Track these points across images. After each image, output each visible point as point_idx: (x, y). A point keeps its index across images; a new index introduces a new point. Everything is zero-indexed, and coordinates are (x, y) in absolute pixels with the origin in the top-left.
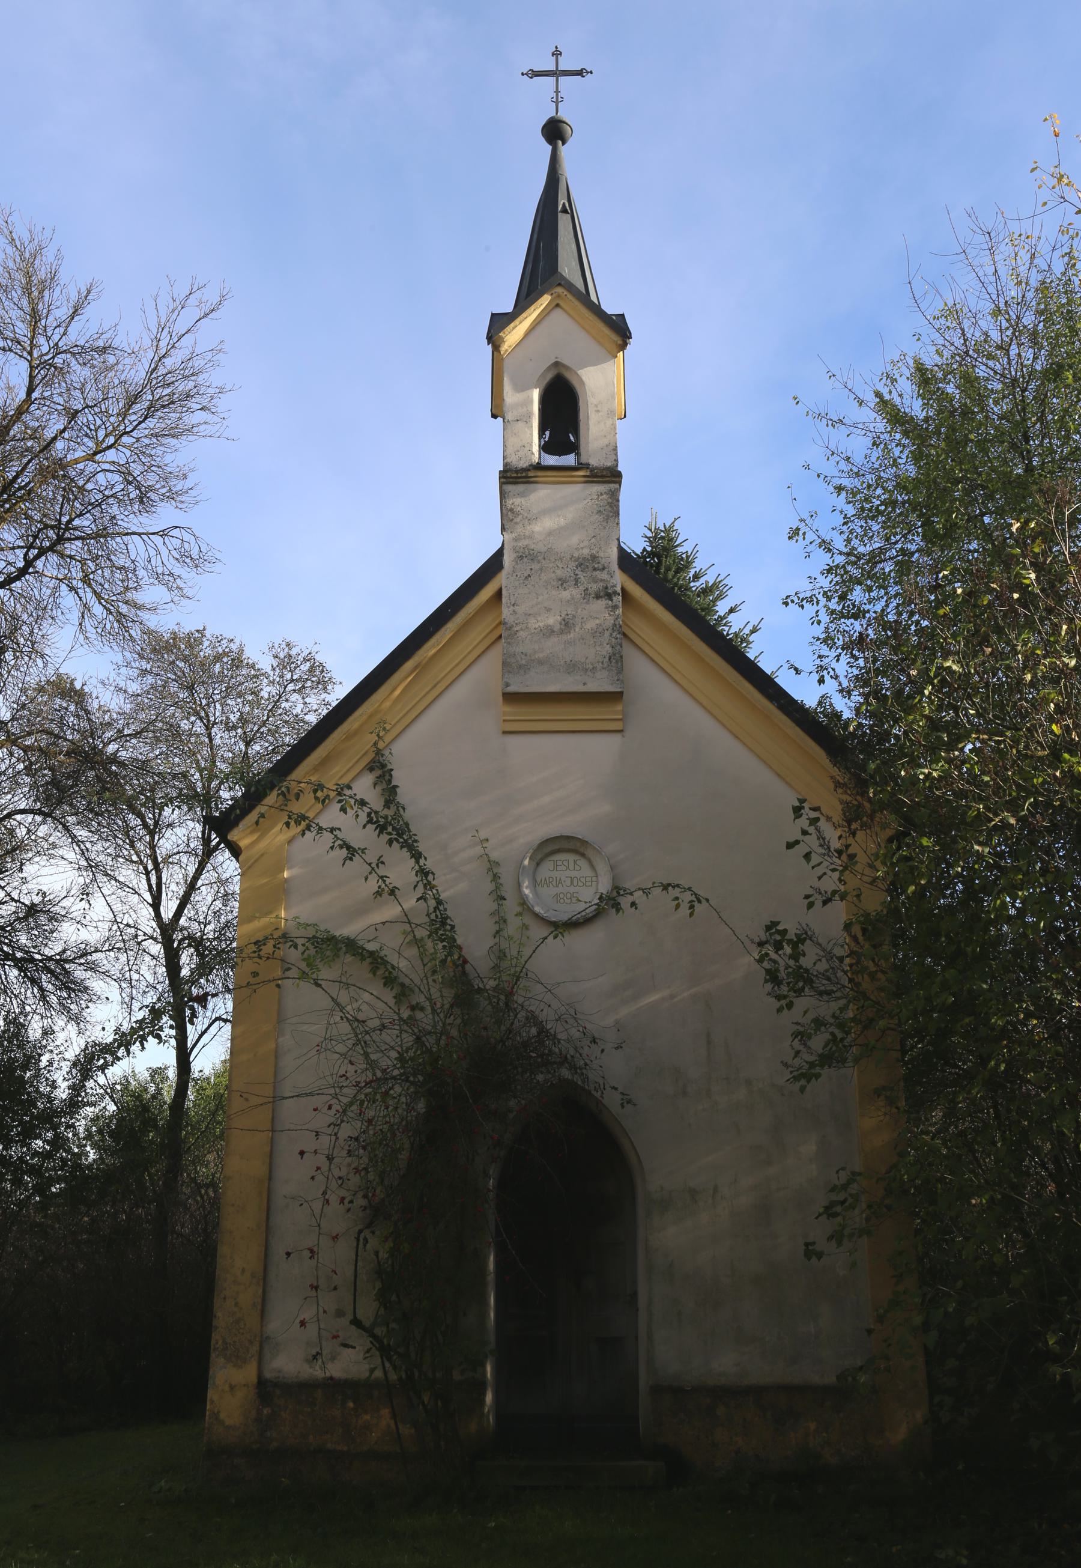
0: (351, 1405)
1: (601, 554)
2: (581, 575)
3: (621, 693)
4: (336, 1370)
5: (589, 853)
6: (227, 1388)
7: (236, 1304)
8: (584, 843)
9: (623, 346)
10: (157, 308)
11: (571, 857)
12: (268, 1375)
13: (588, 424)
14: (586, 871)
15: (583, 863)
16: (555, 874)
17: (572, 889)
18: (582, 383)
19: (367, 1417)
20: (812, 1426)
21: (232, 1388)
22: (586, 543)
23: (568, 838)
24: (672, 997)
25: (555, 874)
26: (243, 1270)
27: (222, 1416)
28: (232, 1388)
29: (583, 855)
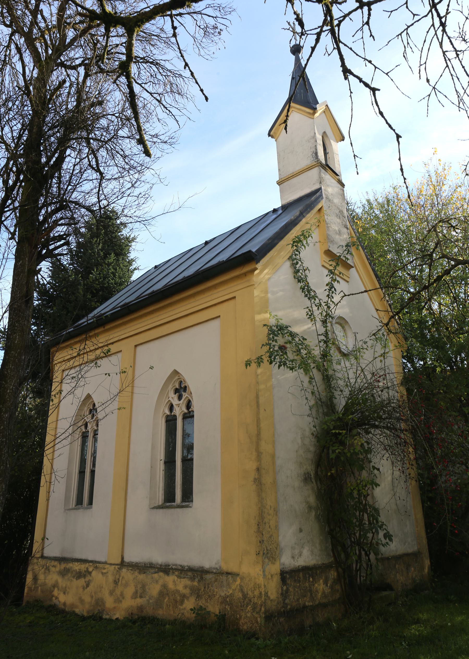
6: (270, 577)
21: (272, 576)
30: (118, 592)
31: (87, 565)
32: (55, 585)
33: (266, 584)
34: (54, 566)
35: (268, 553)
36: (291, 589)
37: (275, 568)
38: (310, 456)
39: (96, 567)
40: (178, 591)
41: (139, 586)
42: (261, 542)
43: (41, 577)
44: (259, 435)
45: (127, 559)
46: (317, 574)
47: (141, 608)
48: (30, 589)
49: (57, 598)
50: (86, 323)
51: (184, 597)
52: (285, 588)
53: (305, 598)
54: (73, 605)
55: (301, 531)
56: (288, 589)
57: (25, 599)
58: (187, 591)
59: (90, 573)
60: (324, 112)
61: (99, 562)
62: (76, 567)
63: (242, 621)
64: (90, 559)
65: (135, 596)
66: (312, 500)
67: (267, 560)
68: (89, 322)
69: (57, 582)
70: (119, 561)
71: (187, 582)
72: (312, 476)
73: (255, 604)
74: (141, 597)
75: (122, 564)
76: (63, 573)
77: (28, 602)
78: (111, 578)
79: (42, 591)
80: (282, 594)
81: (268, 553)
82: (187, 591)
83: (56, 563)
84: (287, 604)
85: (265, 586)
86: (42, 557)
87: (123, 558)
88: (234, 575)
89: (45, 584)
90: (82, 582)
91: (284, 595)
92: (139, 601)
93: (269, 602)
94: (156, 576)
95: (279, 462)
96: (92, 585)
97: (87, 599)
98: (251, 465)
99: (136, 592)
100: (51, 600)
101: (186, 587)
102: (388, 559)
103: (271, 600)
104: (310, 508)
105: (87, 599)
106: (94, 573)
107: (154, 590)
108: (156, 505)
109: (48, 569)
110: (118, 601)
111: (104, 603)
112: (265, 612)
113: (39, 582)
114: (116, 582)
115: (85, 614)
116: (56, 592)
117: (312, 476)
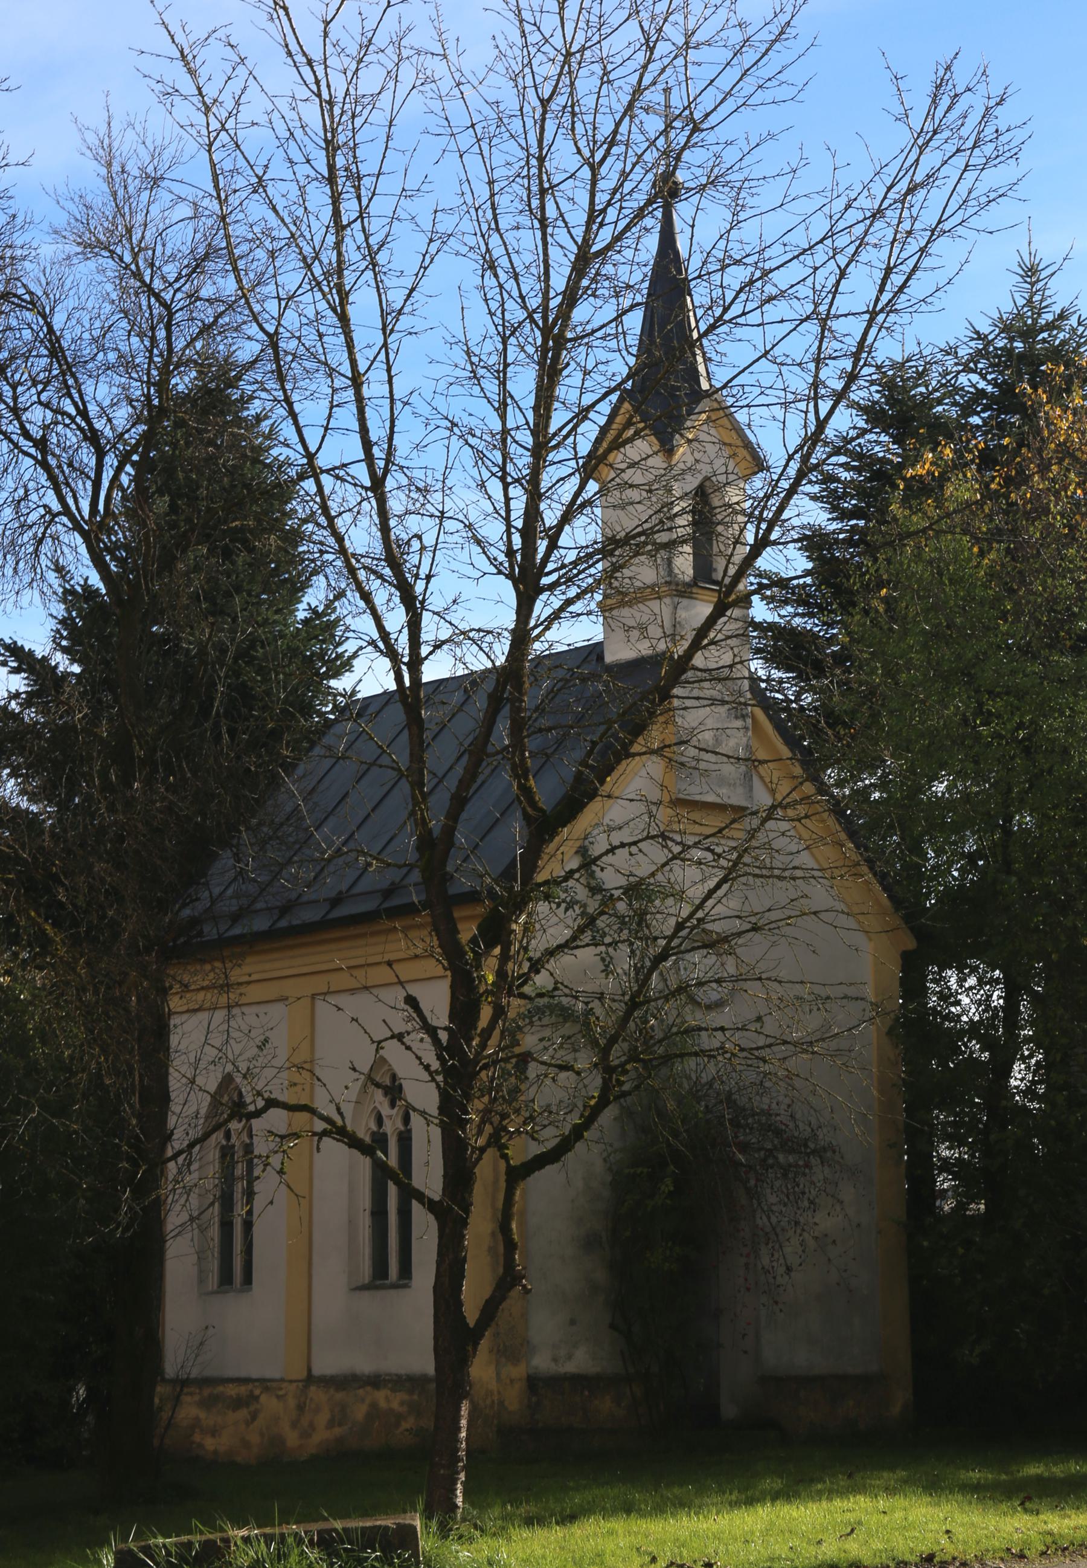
0: (586, 1393)
7: (511, 1315)
28: (512, 1381)
31: (250, 1386)
37: (518, 1371)
52: (534, 1399)
55: (573, 1322)
74: (340, 1425)
75: (310, 1379)
76: (207, 1403)
85: (499, 1393)
87: (309, 1370)
92: (337, 1431)
94: (361, 1392)
101: (402, 1404)
106: (263, 1398)
107: (360, 1412)
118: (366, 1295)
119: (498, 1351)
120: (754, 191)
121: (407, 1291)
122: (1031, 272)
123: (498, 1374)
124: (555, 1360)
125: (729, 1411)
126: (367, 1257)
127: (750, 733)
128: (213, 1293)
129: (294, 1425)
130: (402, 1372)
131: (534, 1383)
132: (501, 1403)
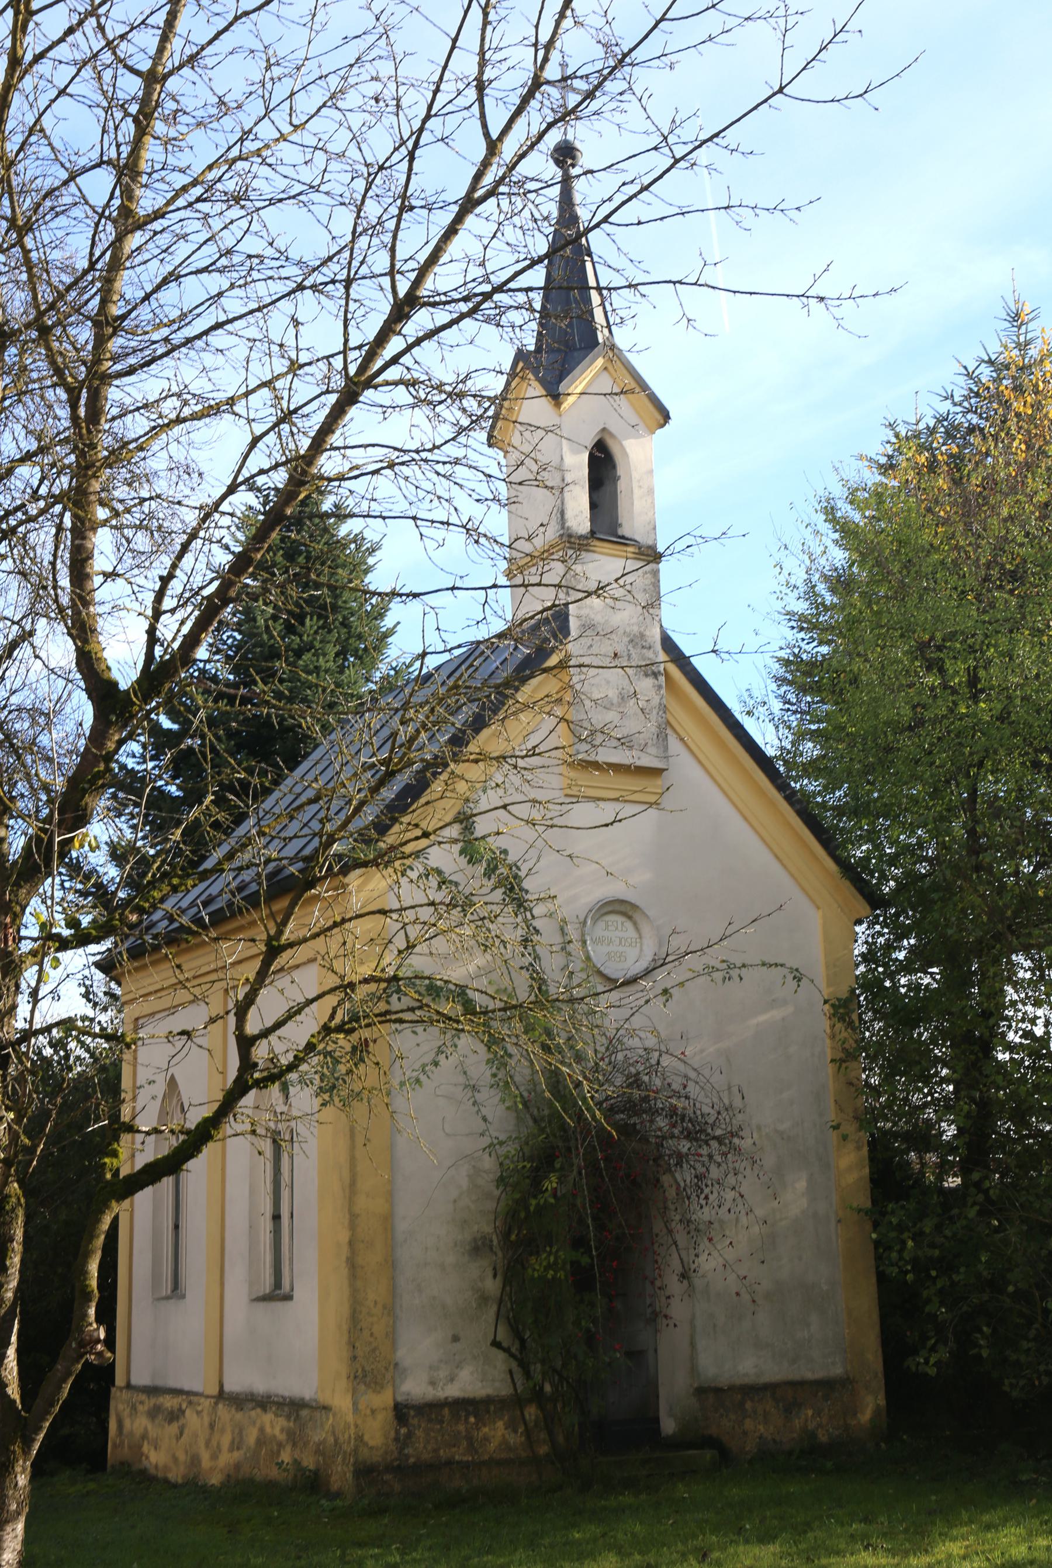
0: (472, 1420)
1: (647, 633)
2: (632, 651)
3: (664, 770)
4: (453, 1391)
5: (637, 916)
6: (368, 1412)
7: (372, 1335)
8: (634, 907)
9: (662, 426)
10: (662, 219)
11: (620, 919)
12: (399, 1399)
13: (632, 498)
14: (630, 932)
15: (629, 924)
16: (606, 933)
17: (621, 949)
18: (625, 454)
19: (486, 1430)
20: (810, 1412)
21: (373, 1412)
22: (634, 620)
23: (622, 902)
24: (702, 1051)
25: (606, 933)
26: (376, 1303)
27: (366, 1438)
28: (373, 1412)
29: (630, 918)
30: (214, 1443)
31: (180, 1399)
32: (144, 1436)
33: (359, 1422)
34: (142, 1403)
35: (365, 1376)
36: (419, 1433)
37: (385, 1399)
38: (491, 1205)
39: (190, 1403)
40: (275, 1436)
41: (237, 1431)
42: (354, 1358)
43: (127, 1423)
44: (353, 1183)
45: (227, 1388)
46: (488, 1412)
47: (237, 1466)
48: (115, 1445)
49: (147, 1458)
50: (592, 283)
51: (280, 1445)
52: (403, 1431)
53: (454, 1450)
54: (166, 1468)
55: (456, 1339)
56: (409, 1435)
57: (109, 1463)
58: (282, 1437)
59: (183, 1412)
60: (606, 369)
61: (196, 1394)
62: (169, 1402)
63: (333, 1479)
64: (186, 1388)
65: (231, 1450)
66: (492, 1286)
67: (362, 1387)
68: (594, 295)
69: (146, 1429)
70: (214, 1391)
71: (282, 1422)
72: (495, 1242)
73: (345, 1452)
74: (238, 1449)
75: (221, 1395)
76: (154, 1413)
77: (113, 1466)
78: (206, 1420)
79: (130, 1447)
80: (396, 1439)
81: (365, 1376)
82: (282, 1437)
83: (143, 1397)
84: (407, 1457)
85: (356, 1426)
86: (129, 1386)
87: (221, 1386)
88: (326, 1408)
89: (131, 1433)
90: (174, 1428)
91: (402, 1442)
92: (237, 1455)
93: (366, 1450)
94: (253, 1413)
95: (402, 1226)
96: (186, 1431)
97: (182, 1457)
98: (344, 1236)
99: (233, 1442)
100: (140, 1461)
101: (282, 1430)
102: (718, 1390)
103: (371, 1448)
104: (484, 1299)
105: (182, 1457)
106: (188, 1413)
107: (251, 1437)
108: (261, 1294)
109: (134, 1408)
110: (214, 1457)
111: (200, 1462)
112: (355, 1463)
113: (125, 1431)
114: (212, 1426)
115: (180, 1481)
116: (145, 1448)
117: (495, 1242)
118: (262, 1305)
119: (355, 1377)
120: (623, 105)
121: (288, 1305)
122: (1016, 318)
123: (355, 1404)
124: (433, 1383)
125: (668, 1426)
126: (268, 1266)
127: (663, 691)
128: (167, 1298)
129: (208, 1444)
130: (286, 1394)
131: (401, 1412)
132: (360, 1438)
